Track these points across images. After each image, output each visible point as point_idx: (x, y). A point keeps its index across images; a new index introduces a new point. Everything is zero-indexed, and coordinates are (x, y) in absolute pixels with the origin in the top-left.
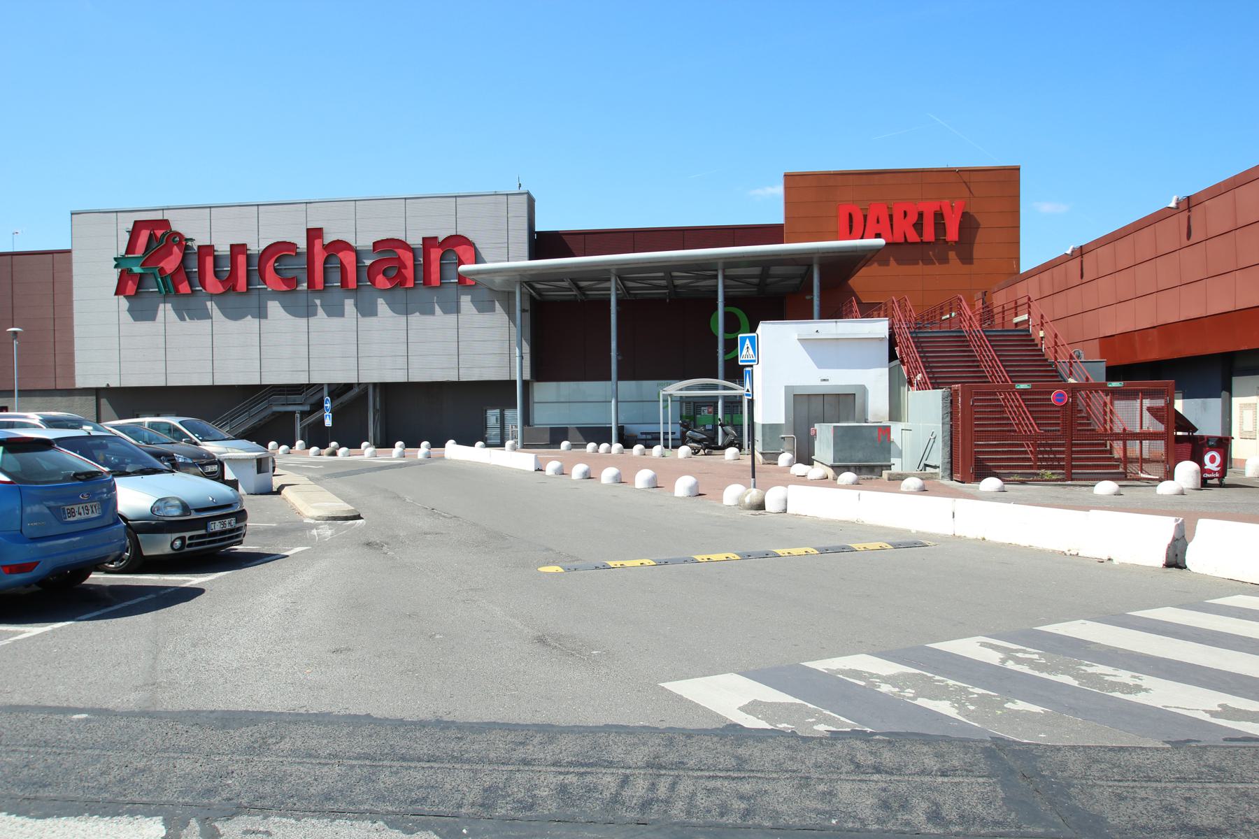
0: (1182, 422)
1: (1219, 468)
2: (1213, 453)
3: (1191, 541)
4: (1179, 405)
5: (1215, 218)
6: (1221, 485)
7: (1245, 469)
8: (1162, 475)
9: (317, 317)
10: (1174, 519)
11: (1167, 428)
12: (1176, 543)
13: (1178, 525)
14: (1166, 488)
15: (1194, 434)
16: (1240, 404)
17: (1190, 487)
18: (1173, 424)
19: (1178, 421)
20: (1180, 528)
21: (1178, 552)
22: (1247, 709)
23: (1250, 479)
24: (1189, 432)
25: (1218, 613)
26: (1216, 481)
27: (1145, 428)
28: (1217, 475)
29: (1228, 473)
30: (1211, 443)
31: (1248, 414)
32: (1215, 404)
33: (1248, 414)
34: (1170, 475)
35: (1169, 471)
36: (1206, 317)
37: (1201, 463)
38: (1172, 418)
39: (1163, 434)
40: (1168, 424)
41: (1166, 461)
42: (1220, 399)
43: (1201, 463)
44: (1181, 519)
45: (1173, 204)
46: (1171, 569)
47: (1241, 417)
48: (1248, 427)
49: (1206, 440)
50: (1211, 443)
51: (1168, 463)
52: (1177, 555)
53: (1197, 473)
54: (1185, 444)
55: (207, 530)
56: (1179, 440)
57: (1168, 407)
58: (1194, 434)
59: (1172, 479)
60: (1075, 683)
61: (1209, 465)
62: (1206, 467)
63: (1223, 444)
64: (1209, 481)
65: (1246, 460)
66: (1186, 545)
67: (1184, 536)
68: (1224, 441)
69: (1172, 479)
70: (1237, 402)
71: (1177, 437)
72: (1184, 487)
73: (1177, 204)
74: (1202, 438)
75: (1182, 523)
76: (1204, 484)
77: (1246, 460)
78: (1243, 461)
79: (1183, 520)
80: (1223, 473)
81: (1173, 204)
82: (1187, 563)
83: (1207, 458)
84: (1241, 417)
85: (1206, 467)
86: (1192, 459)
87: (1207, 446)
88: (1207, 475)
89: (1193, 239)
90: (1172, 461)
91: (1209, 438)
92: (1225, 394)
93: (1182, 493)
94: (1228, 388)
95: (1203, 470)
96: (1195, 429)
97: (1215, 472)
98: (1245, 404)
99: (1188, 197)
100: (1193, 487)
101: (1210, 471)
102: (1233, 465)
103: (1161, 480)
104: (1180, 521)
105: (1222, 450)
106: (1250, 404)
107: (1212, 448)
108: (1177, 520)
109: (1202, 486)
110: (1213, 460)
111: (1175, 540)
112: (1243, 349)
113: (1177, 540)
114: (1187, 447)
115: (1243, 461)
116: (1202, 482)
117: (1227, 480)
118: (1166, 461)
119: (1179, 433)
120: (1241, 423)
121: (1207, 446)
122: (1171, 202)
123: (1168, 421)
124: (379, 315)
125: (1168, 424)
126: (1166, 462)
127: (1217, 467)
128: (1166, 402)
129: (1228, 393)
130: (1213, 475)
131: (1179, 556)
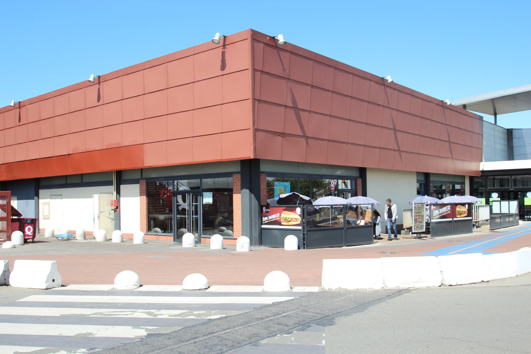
0: (15, 212)
1: (32, 234)
2: (29, 226)
3: (12, 271)
4: (15, 203)
5: (30, 114)
6: (33, 242)
7: (44, 233)
8: (6, 239)
9: (201, 244)
10: (3, 261)
11: (8, 215)
12: (5, 273)
13: (6, 264)
14: (7, 245)
15: (21, 217)
16: (43, 203)
17: (19, 244)
18: (10, 213)
19: (13, 211)
20: (7, 265)
21: (6, 278)
22: (27, 352)
23: (47, 238)
24: (18, 217)
25: (21, 306)
26: (31, 240)
27: (173, 235)
28: (31, 237)
29: (36, 236)
30: (28, 222)
31: (46, 207)
32: (32, 202)
33: (46, 207)
34: (9, 238)
35: (9, 236)
36: (27, 161)
37: (24, 232)
38: (10, 210)
39: (5, 218)
40: (8, 213)
41: (7, 231)
42: (34, 200)
43: (24, 232)
44: (7, 261)
45: (12, 104)
46: (2, 286)
47: (43, 209)
48: (46, 213)
49: (26, 220)
50: (28, 222)
51: (8, 232)
52: (5, 279)
53: (22, 237)
54: (16, 223)
55: (321, 285)
56: (13, 220)
57: (8, 204)
58: (21, 217)
59: (10, 240)
60: (195, 318)
61: (27, 233)
62: (26, 234)
63: (34, 222)
64: (28, 240)
65: (76, 231)
66: (10, 273)
67: (9, 269)
68: (34, 221)
69: (10, 240)
70: (41, 201)
71: (13, 219)
72: (16, 244)
73: (14, 104)
74: (24, 219)
75: (8, 263)
76: (26, 241)
77: (76, 231)
78: (44, 230)
79: (8, 261)
80: (34, 236)
81: (12, 104)
82: (11, 283)
83: (26, 229)
84: (43, 209)
85: (26, 234)
86: (20, 230)
87: (26, 223)
88: (27, 237)
89: (22, 123)
90: (10, 231)
91: (27, 220)
92: (36, 198)
93: (14, 247)
94: (37, 195)
95: (25, 235)
96: (21, 215)
97: (30, 236)
98: (45, 203)
99: (20, 102)
100: (20, 244)
101: (28, 235)
102: (40, 232)
103: (5, 241)
104: (7, 262)
105: (33, 225)
106: (47, 203)
107: (29, 224)
108: (5, 262)
109: (24, 243)
110: (29, 230)
111: (4, 272)
112: (43, 177)
113: (5, 271)
114: (17, 224)
115: (44, 230)
116: (24, 241)
117: (36, 239)
118: (7, 231)
119: (14, 217)
120: (43, 212)
121: (26, 223)
122: (11, 103)
123: (8, 211)
124: (93, 231)
125: (8, 213)
126: (7, 232)
127: (31, 233)
128: (7, 201)
129: (37, 197)
130: (29, 237)
131: (6, 280)
